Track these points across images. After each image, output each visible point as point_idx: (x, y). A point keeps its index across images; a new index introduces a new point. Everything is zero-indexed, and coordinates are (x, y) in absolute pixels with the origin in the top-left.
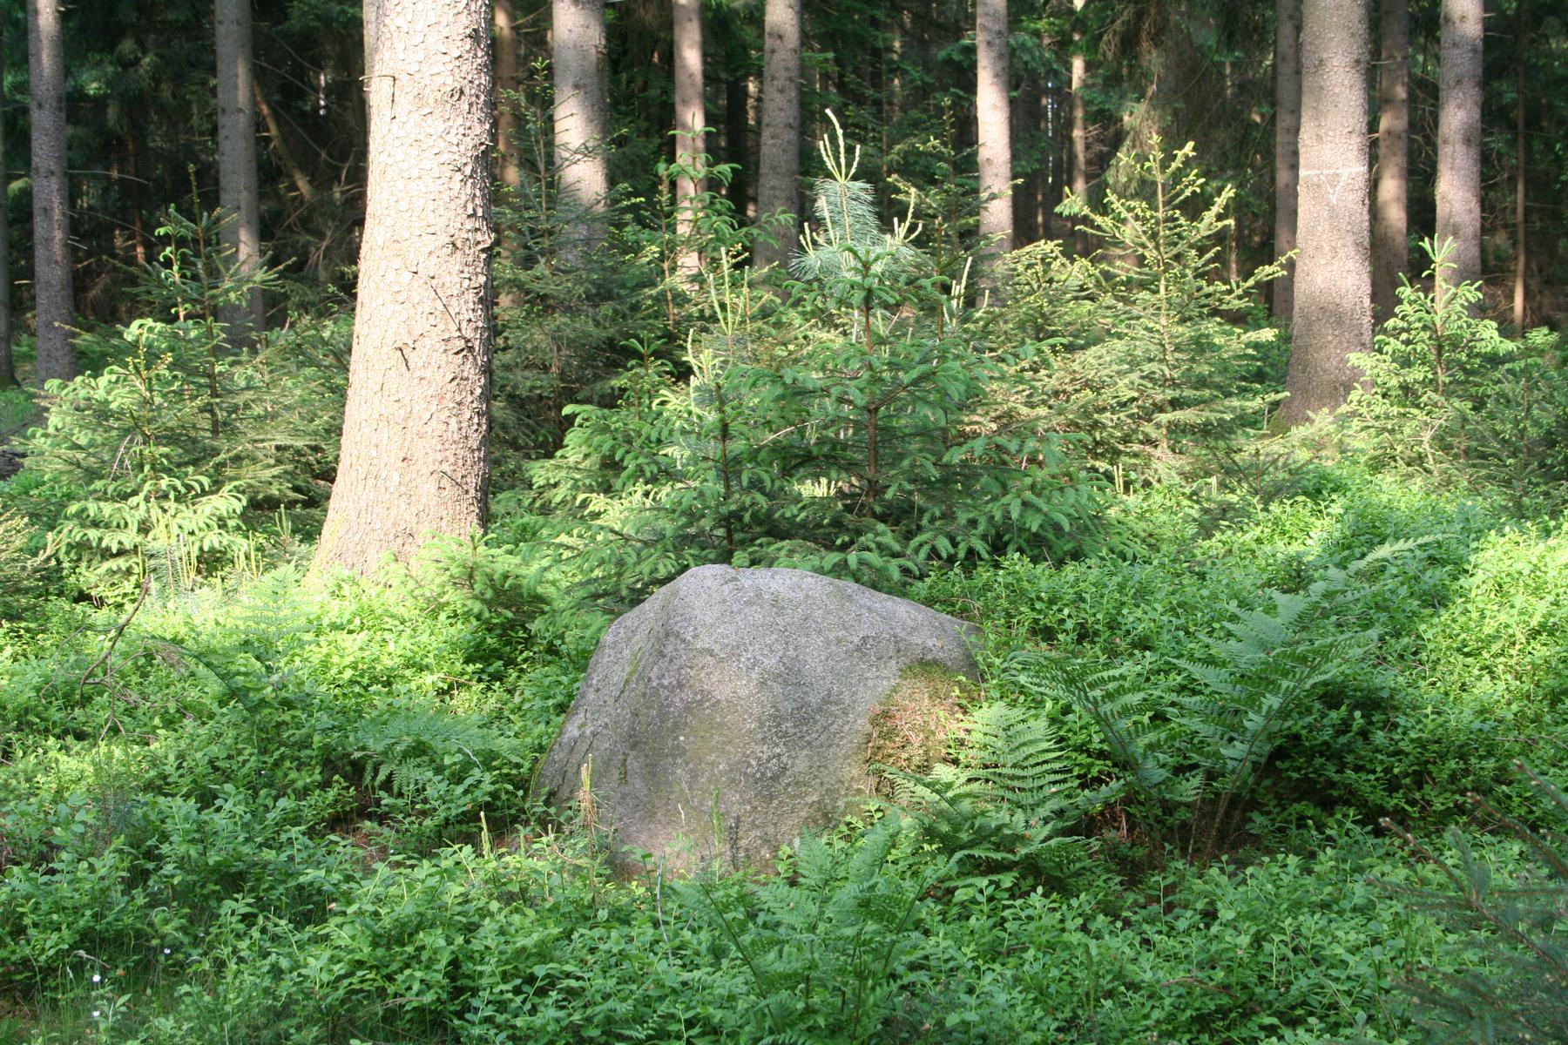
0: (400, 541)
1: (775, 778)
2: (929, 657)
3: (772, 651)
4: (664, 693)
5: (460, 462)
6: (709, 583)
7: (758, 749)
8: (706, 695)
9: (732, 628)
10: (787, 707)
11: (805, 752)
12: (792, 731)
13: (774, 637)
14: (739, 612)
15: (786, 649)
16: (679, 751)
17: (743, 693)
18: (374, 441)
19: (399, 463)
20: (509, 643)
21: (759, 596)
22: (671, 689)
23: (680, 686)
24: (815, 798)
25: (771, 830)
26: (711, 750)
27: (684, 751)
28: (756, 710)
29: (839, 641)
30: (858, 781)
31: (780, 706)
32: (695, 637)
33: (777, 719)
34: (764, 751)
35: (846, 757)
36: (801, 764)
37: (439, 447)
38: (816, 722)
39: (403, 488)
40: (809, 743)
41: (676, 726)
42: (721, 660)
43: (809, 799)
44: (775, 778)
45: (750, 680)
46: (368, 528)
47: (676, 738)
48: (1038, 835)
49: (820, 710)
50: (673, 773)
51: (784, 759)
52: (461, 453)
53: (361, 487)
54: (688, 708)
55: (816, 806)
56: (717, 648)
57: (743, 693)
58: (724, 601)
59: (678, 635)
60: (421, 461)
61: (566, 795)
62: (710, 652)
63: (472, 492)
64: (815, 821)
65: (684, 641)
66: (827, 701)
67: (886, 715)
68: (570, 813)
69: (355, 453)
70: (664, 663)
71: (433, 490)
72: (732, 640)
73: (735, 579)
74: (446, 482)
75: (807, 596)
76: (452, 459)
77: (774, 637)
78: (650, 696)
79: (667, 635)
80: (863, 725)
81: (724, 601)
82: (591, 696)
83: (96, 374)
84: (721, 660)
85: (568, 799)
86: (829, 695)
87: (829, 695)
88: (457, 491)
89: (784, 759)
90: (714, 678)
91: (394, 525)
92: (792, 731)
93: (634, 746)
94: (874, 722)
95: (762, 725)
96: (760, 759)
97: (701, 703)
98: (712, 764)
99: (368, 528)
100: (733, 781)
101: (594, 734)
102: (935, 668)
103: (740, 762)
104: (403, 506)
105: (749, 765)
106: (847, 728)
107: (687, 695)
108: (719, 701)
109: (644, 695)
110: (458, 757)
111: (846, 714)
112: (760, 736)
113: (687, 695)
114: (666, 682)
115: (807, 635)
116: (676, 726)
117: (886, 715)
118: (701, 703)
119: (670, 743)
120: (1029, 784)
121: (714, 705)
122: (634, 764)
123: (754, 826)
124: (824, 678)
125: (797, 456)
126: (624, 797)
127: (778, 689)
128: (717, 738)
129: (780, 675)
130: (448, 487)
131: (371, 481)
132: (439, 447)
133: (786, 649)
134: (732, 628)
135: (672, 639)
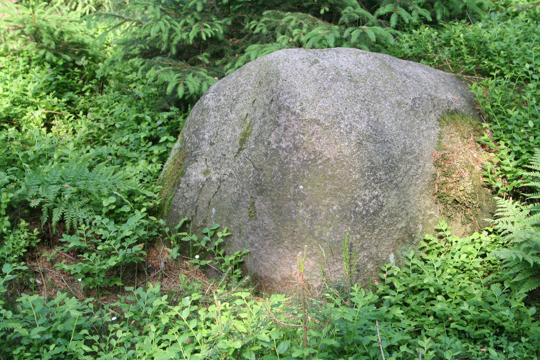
2: (452, 108)
3: (361, 118)
6: (300, 65)
7: (362, 193)
8: (318, 155)
9: (329, 101)
10: (379, 160)
11: (394, 192)
12: (384, 177)
13: (359, 106)
16: (299, 197)
21: (338, 73)
22: (289, 150)
23: (296, 148)
24: (403, 224)
25: (374, 250)
28: (358, 164)
30: (430, 209)
31: (374, 159)
32: (303, 110)
33: (373, 169)
34: (367, 194)
35: (421, 193)
38: (399, 169)
40: (396, 185)
41: (296, 178)
42: (326, 128)
43: (399, 226)
44: (375, 213)
45: (350, 142)
48: (79, 19)
49: (401, 159)
51: (381, 199)
54: (304, 164)
55: (404, 230)
56: (321, 118)
57: (347, 152)
58: (316, 80)
59: (288, 109)
61: (200, 223)
62: (317, 122)
64: (404, 241)
65: (294, 113)
66: (404, 152)
67: (444, 158)
70: (280, 131)
72: (331, 111)
73: (316, 61)
77: (359, 106)
79: (280, 109)
80: (430, 168)
82: (206, 148)
84: (326, 128)
85: (202, 227)
89: (381, 199)
90: (323, 141)
93: (261, 192)
96: (364, 200)
98: (327, 205)
101: (221, 181)
102: (457, 116)
103: (350, 203)
105: (357, 206)
106: (420, 171)
107: (303, 155)
108: (329, 159)
109: (266, 155)
110: (113, 200)
111: (418, 161)
112: (362, 184)
113: (303, 155)
114: (284, 145)
115: (379, 102)
116: (296, 178)
118: (314, 161)
121: (325, 162)
122: (261, 204)
123: (362, 248)
124: (398, 135)
126: (254, 229)
127: (371, 147)
128: (330, 187)
129: (370, 136)
134: (329, 101)
135: (284, 112)
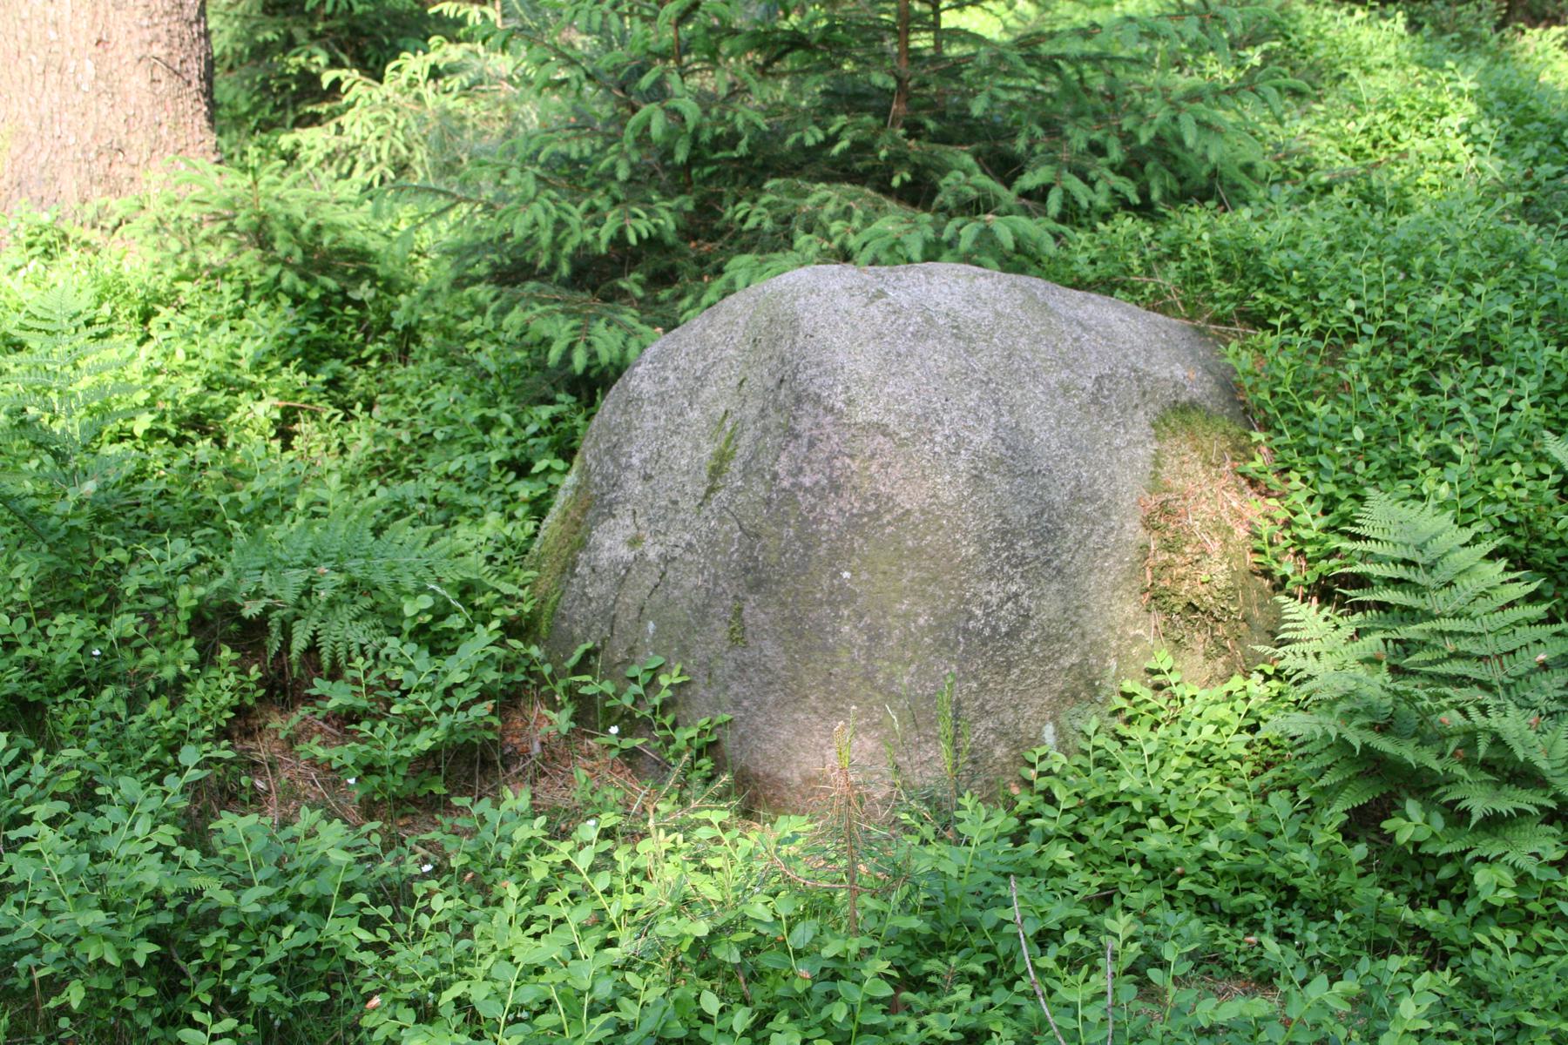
0: (105, 160)
1: (1013, 634)
2: (1184, 398)
3: (980, 420)
4: (806, 500)
5: (177, 41)
6: (843, 302)
7: (982, 588)
8: (884, 502)
10: (1020, 513)
11: (1055, 586)
12: (1031, 553)
13: (975, 393)
14: (910, 353)
15: (999, 414)
16: (841, 597)
17: (948, 496)
18: (51, 17)
19: (92, 49)
20: (332, 327)
21: (929, 321)
23: (836, 488)
24: (1074, 659)
25: (1009, 716)
26: (902, 594)
27: (851, 598)
28: (973, 524)
29: (1066, 389)
30: (1134, 623)
31: (1008, 513)
32: (850, 402)
33: (1007, 534)
35: (1115, 588)
36: (1051, 607)
37: (145, 22)
39: (102, 84)
40: (1059, 571)
42: (903, 443)
43: (1066, 662)
44: (1013, 634)
45: (956, 474)
46: (57, 145)
47: (836, 574)
50: (836, 632)
51: (1024, 601)
52: (176, 28)
53: (38, 86)
54: (854, 524)
56: (892, 421)
58: (880, 335)
59: (817, 400)
60: (122, 44)
61: (620, 655)
62: (883, 429)
63: (195, 82)
64: (1075, 696)
65: (830, 410)
66: (1076, 497)
67: (1165, 510)
68: (637, 689)
69: (23, 35)
70: (799, 448)
71: (144, 84)
72: (914, 405)
73: (881, 294)
74: (160, 73)
75: (998, 314)
76: (165, 38)
77: (975, 393)
78: (782, 503)
81: (880, 335)
82: (636, 487)
83: (1548, 27)
85: (626, 663)
86: (1078, 487)
87: (1078, 487)
88: (177, 83)
89: (1024, 601)
90: (896, 472)
91: (94, 137)
92: (1031, 553)
93: (756, 586)
94: (1149, 524)
95: (984, 549)
96: (987, 604)
97: (875, 516)
98: (905, 616)
99: (57, 145)
100: (945, 642)
103: (955, 611)
104: (105, 111)
105: (971, 616)
110: (426, 601)
111: (1107, 516)
112: (983, 567)
114: (807, 481)
115: (1021, 385)
117: (1165, 510)
118: (875, 516)
119: (825, 582)
120: (1488, 647)
121: (899, 519)
122: (757, 613)
123: (983, 712)
124: (1064, 458)
125: (783, 42)
126: (742, 667)
127: (1002, 485)
129: (1000, 461)
130: (164, 78)
131: (53, 77)
132: (145, 22)
133: (999, 414)
135: (808, 407)
